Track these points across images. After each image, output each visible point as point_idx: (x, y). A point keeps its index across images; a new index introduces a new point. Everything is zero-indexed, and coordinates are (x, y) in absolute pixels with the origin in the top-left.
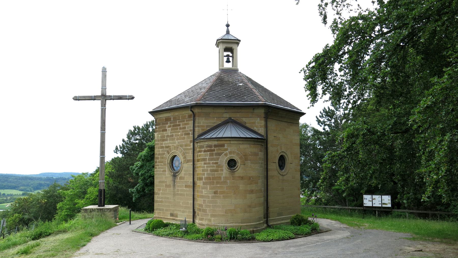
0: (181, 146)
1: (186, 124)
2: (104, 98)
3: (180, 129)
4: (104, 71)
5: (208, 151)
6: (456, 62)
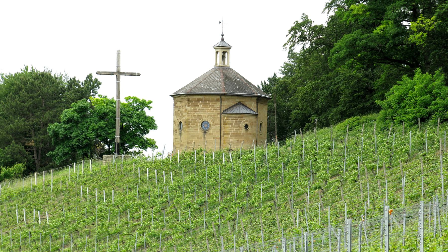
0: (211, 116)
1: (214, 104)
2: (119, 74)
3: (210, 106)
4: (119, 53)
5: (234, 120)
6: (297, 248)
